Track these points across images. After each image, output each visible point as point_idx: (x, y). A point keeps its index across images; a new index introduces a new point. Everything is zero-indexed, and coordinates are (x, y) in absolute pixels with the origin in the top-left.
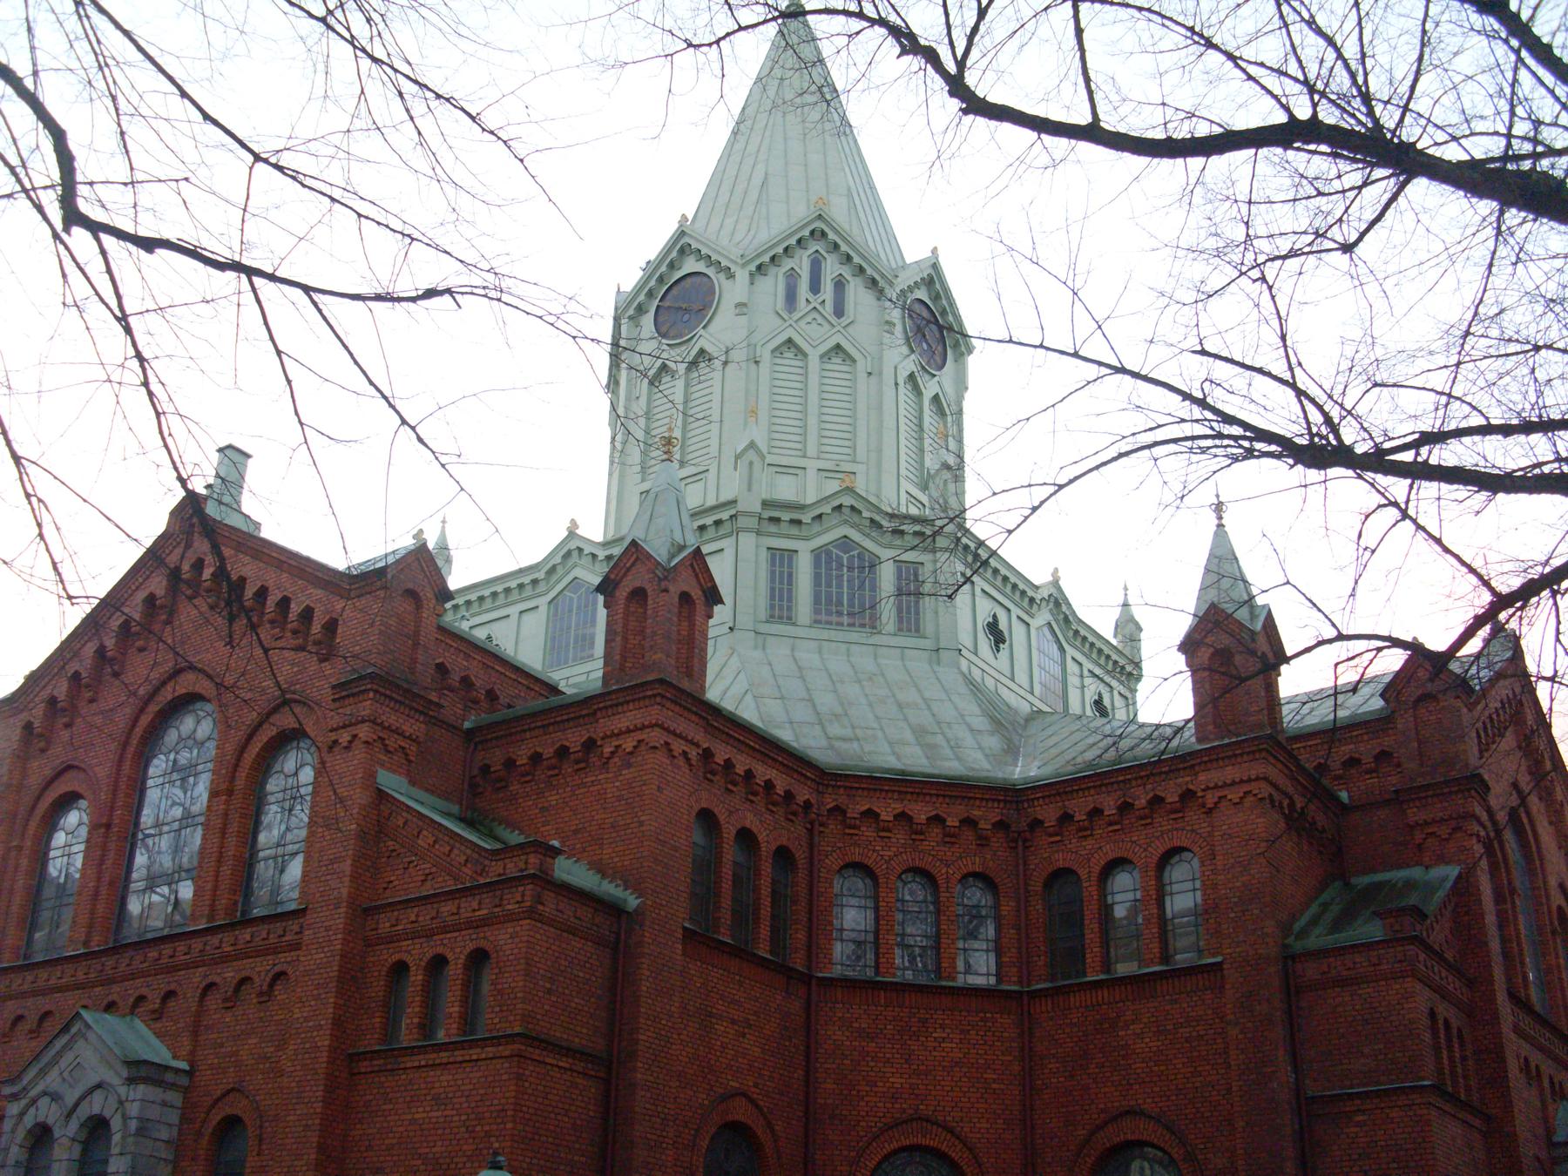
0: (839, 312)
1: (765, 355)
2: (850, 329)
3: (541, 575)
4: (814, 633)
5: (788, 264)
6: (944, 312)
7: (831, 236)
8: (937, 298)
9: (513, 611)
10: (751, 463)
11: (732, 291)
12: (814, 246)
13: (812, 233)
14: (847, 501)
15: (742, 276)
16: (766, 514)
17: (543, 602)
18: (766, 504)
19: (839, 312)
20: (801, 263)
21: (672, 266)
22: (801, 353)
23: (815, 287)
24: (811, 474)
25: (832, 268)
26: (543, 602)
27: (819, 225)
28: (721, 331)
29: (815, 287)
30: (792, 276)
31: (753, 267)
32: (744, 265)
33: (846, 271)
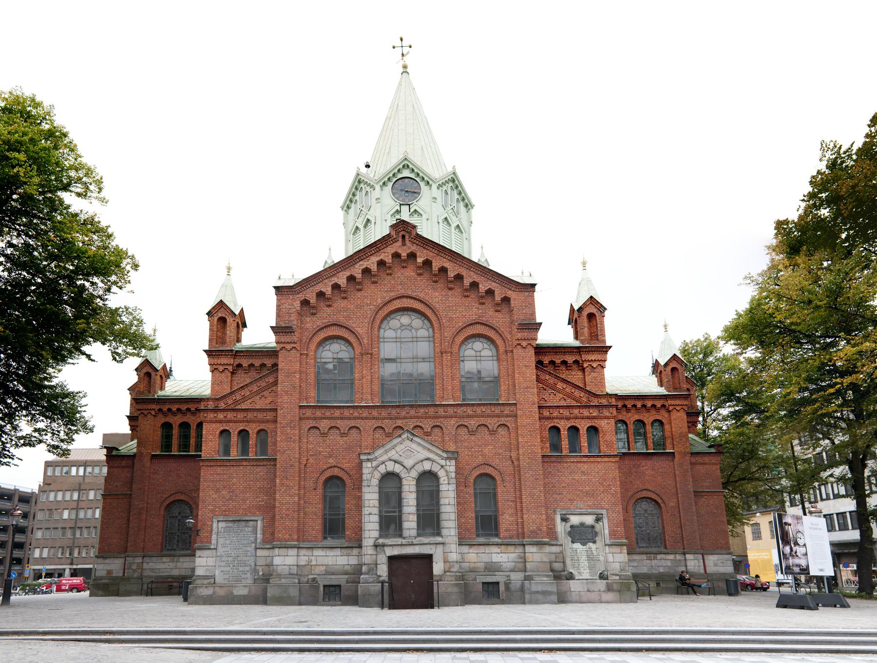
1: (441, 221)
13: (404, 166)
15: (378, 187)
27: (406, 162)
31: (381, 183)
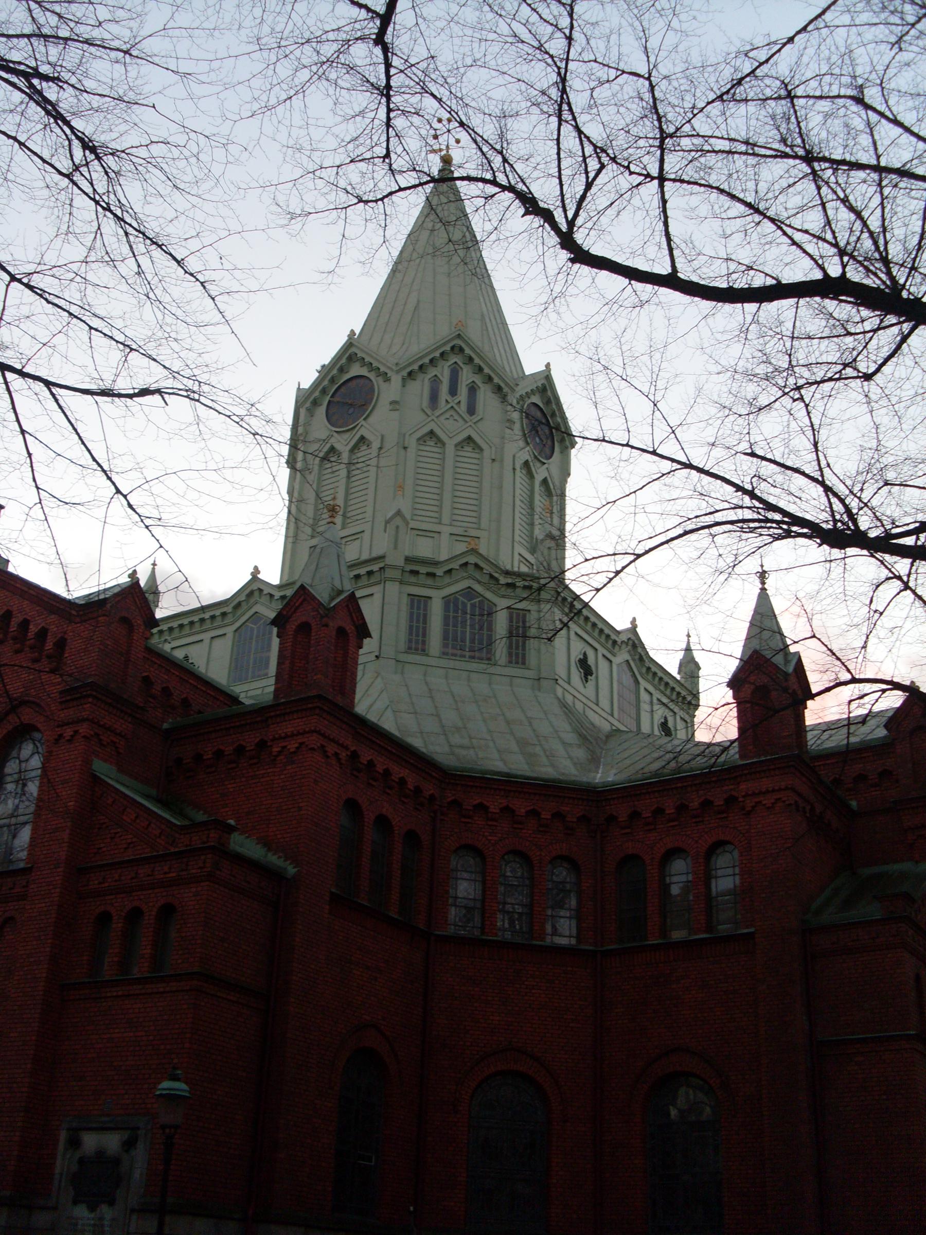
0: (471, 410)
1: (412, 443)
2: (480, 425)
3: (228, 609)
4: (443, 662)
5: (432, 372)
6: (553, 415)
7: (468, 351)
8: (548, 402)
9: (206, 636)
10: (397, 527)
11: (389, 391)
12: (454, 359)
13: (453, 348)
14: (472, 559)
15: (396, 380)
16: (409, 568)
17: (230, 630)
18: (408, 560)
19: (471, 410)
20: (443, 371)
21: (342, 370)
22: (440, 442)
23: (453, 391)
24: (445, 538)
25: (467, 376)
26: (230, 630)
27: (458, 342)
28: (379, 423)
29: (453, 391)
30: (436, 381)
31: (405, 373)
32: (398, 372)
33: (478, 379)
